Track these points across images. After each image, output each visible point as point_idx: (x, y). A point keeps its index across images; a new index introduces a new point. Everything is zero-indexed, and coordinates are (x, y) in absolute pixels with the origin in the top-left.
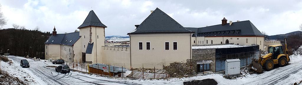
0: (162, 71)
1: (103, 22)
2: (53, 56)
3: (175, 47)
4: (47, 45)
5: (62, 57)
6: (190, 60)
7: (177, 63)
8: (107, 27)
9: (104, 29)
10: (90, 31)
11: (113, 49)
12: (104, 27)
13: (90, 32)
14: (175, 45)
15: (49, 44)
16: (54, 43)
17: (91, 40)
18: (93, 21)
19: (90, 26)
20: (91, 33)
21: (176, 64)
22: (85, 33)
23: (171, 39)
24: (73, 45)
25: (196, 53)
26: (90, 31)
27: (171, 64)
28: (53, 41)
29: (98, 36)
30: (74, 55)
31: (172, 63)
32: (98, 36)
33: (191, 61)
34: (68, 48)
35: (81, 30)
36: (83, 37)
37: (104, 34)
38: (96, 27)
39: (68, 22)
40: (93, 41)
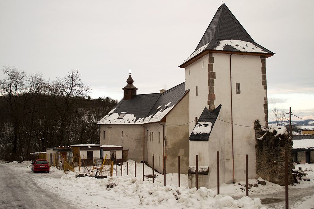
8: (272, 54)
9: (263, 61)
17: (212, 98)
20: (212, 75)
26: (211, 67)
29: (238, 85)
32: (238, 85)
35: (188, 70)
36: (192, 93)
40: (221, 99)
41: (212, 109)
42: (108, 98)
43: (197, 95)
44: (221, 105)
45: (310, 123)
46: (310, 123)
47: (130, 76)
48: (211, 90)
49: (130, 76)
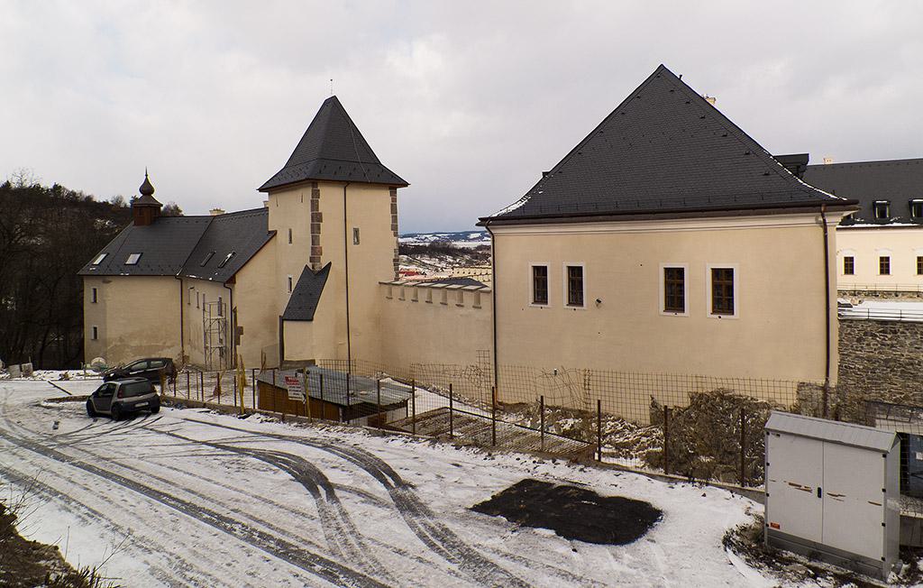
0: (641, 432)
1: (387, 160)
2: (134, 343)
3: (723, 296)
4: (97, 284)
5: (187, 348)
6: (825, 389)
7: (732, 399)
8: (406, 184)
9: (393, 193)
10: (315, 205)
11: (423, 295)
12: (393, 183)
13: (396, 216)
14: (723, 283)
15: (105, 275)
16: (138, 273)
17: (316, 253)
18: (335, 154)
19: (313, 182)
20: (317, 218)
21: (727, 405)
22: (291, 214)
23: (701, 245)
24: (232, 280)
25: (870, 348)
26: (315, 205)
27: (699, 400)
28: (133, 259)
29: (356, 231)
30: (240, 331)
31: (702, 395)
32: (356, 231)
33: (825, 399)
34: (207, 294)
35: (274, 196)
36: (282, 237)
37: (395, 219)
38: (346, 183)
39: (218, 159)
40: (331, 253)
41: (317, 269)
42: (57, 188)
43: (291, 242)
44: (330, 263)
45: (472, 236)
46: (472, 236)
47: (147, 179)
48: (315, 240)
49: (147, 179)
